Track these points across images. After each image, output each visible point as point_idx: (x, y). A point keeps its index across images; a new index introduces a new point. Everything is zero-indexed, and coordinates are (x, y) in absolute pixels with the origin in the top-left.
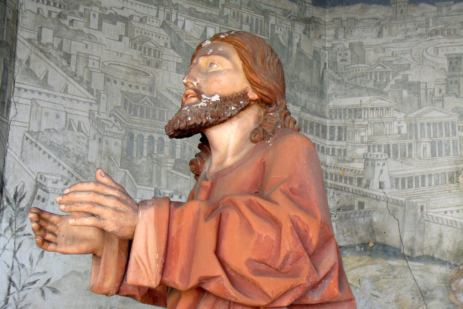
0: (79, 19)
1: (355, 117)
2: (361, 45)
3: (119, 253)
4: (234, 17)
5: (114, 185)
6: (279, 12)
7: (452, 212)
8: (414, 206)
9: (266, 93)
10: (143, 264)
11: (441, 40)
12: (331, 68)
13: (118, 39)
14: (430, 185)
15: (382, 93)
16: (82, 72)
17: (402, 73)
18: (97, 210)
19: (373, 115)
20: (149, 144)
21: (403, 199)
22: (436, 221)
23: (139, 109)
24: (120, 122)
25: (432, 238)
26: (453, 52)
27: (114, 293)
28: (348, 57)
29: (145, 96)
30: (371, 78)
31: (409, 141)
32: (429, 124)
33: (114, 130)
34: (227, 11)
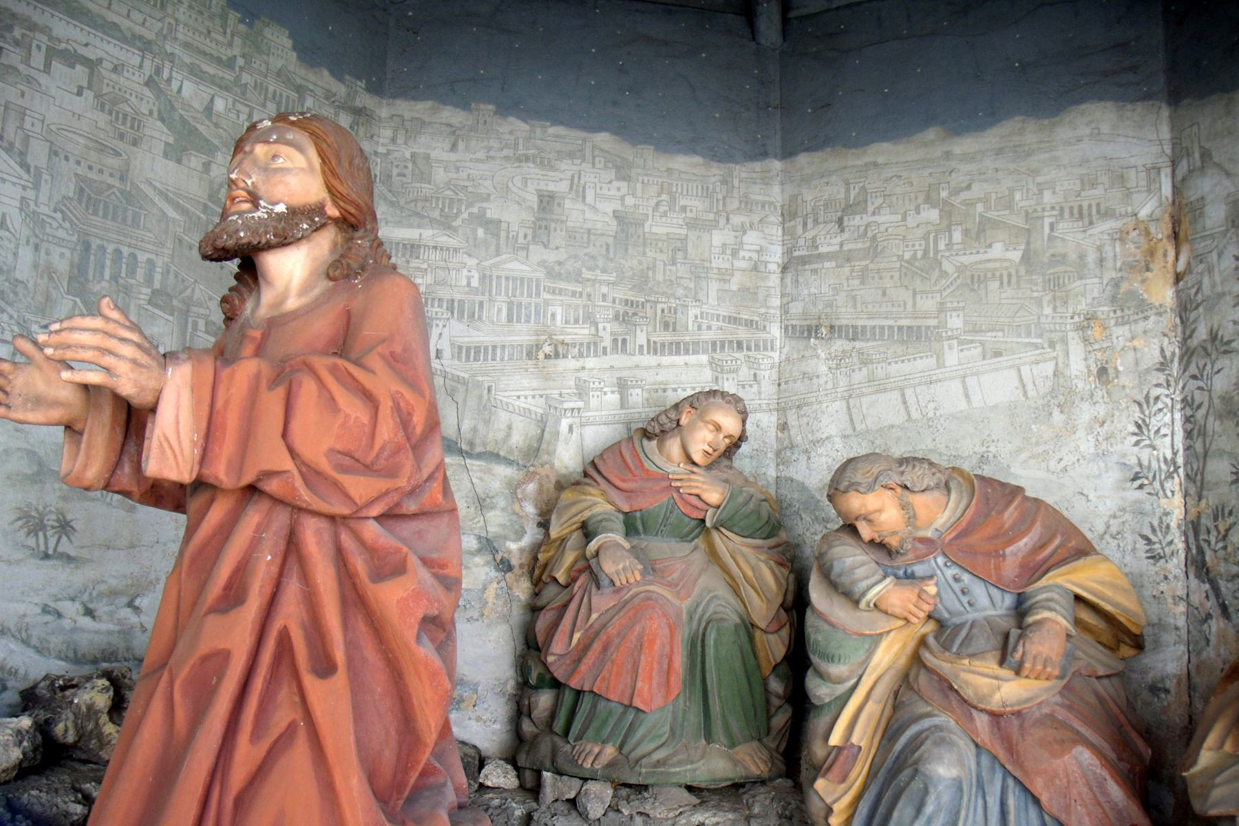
0: (12, 49)
1: (411, 256)
2: (427, 157)
3: (113, 428)
4: (255, 87)
5: (127, 324)
6: (319, 92)
7: (526, 397)
8: (479, 385)
9: (353, 211)
10: (171, 447)
11: (531, 169)
12: (383, 183)
13: (75, 91)
14: (502, 359)
15: (450, 227)
16: (12, 135)
17: (478, 205)
18: (108, 360)
19: (435, 256)
20: (114, 261)
21: (466, 376)
22: (506, 407)
23: (101, 206)
24: (71, 222)
25: (499, 430)
26: (545, 188)
27: (101, 486)
28: (408, 172)
29: (113, 186)
30: (437, 204)
31: (480, 298)
32: (507, 278)
33: (61, 233)
34: (246, 78)
